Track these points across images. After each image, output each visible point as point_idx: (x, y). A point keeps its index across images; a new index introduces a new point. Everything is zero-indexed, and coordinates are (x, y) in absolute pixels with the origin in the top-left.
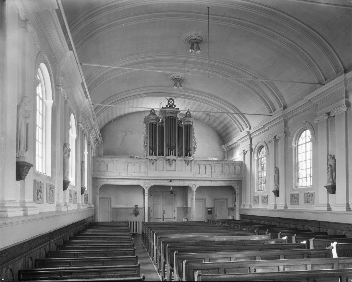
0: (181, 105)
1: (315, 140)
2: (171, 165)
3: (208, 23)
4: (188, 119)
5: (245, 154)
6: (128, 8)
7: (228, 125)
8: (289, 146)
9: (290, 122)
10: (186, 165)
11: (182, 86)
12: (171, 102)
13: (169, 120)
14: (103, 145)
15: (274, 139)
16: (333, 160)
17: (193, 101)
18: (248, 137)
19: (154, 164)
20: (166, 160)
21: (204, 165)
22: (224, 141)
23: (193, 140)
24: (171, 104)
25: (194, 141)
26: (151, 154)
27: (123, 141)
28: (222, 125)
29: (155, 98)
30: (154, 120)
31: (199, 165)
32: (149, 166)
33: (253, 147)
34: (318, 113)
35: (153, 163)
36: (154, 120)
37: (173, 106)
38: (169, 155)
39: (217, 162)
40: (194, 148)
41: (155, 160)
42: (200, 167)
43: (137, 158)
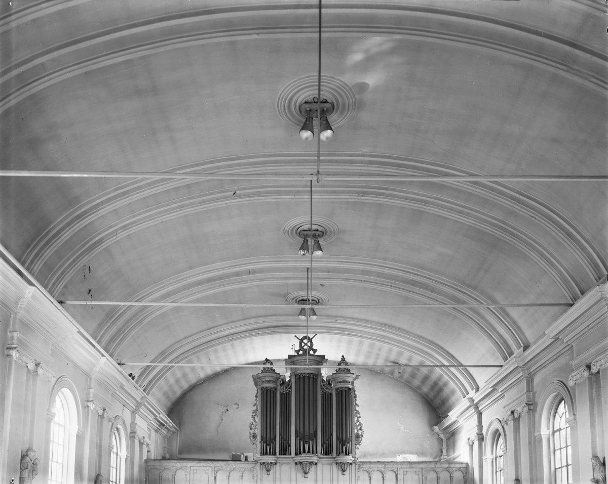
0: (329, 347)
1: (573, 424)
2: (306, 473)
3: (311, 201)
4: (342, 377)
5: (472, 446)
6: (65, 240)
7: (441, 384)
8: (536, 434)
9: (537, 379)
10: (340, 472)
11: (315, 314)
12: (306, 344)
13: (302, 380)
14: (179, 432)
15: (511, 417)
16: (602, 468)
17: (356, 339)
18: (473, 410)
19: (271, 472)
20: (296, 464)
21: (379, 473)
22: (439, 417)
23: (356, 419)
24: (306, 347)
25: (358, 421)
26: (264, 453)
27: (221, 422)
28: (430, 383)
29: (277, 336)
30: (269, 381)
31: (369, 473)
32: (259, 477)
33: (484, 432)
34: (574, 363)
35: (268, 471)
36: (269, 381)
37: (311, 352)
38: (300, 453)
39: (409, 466)
40: (358, 437)
41: (271, 463)
42: (383, 477)
43: (246, 459)
